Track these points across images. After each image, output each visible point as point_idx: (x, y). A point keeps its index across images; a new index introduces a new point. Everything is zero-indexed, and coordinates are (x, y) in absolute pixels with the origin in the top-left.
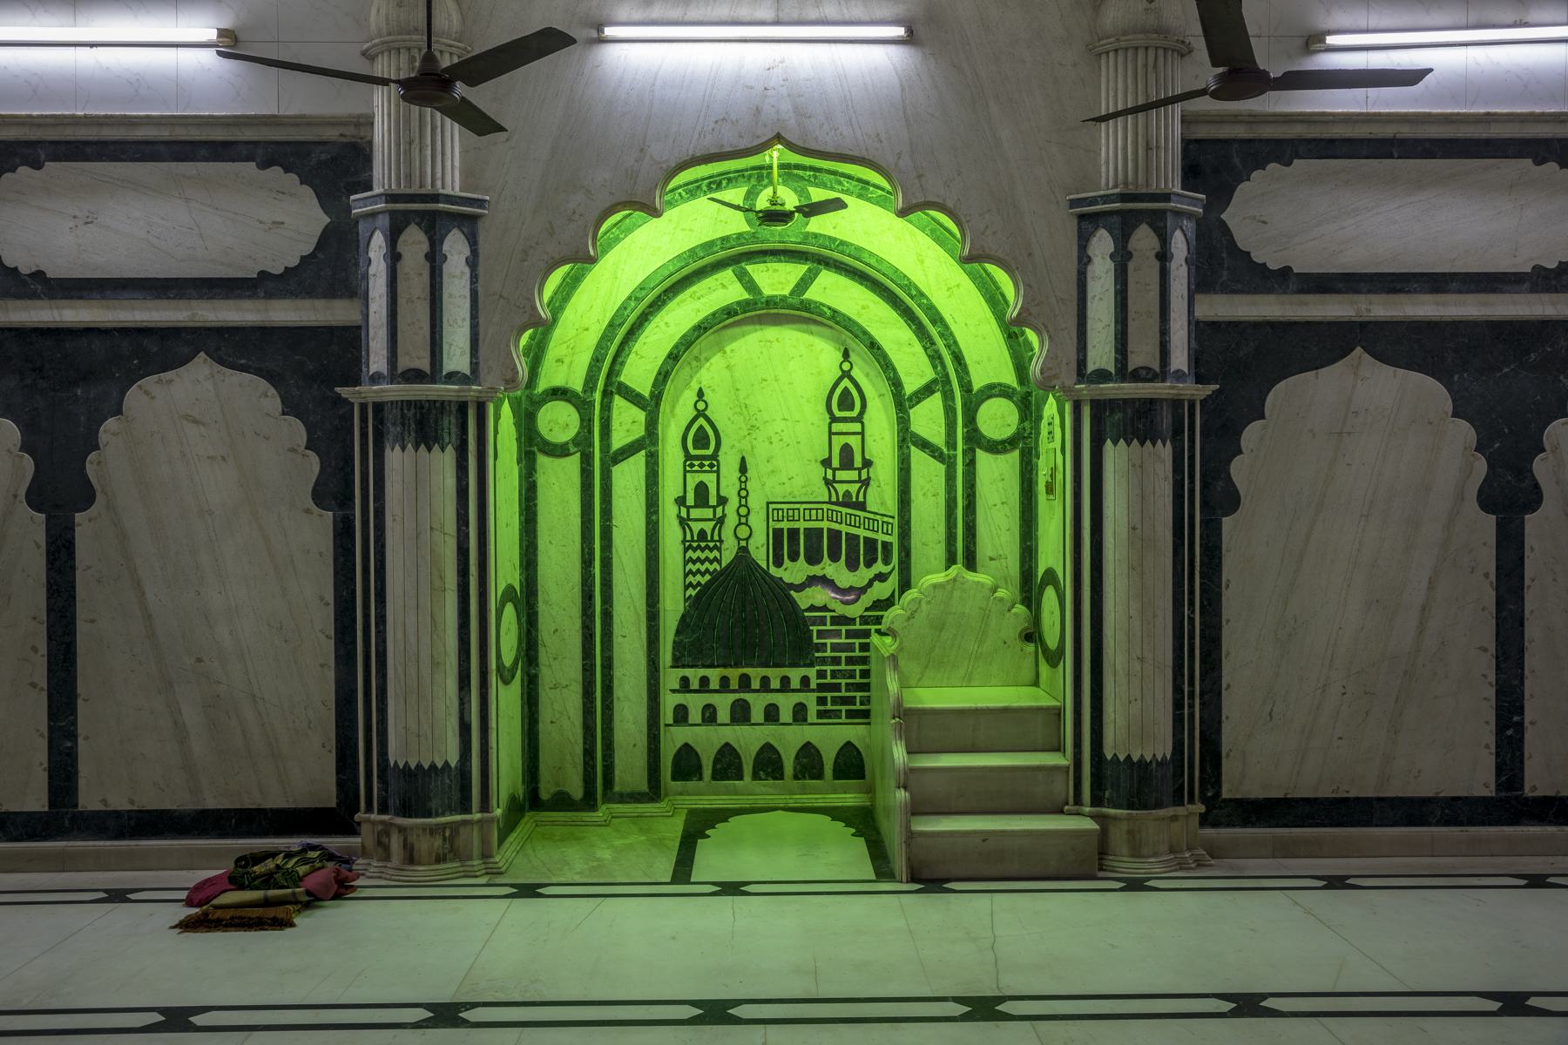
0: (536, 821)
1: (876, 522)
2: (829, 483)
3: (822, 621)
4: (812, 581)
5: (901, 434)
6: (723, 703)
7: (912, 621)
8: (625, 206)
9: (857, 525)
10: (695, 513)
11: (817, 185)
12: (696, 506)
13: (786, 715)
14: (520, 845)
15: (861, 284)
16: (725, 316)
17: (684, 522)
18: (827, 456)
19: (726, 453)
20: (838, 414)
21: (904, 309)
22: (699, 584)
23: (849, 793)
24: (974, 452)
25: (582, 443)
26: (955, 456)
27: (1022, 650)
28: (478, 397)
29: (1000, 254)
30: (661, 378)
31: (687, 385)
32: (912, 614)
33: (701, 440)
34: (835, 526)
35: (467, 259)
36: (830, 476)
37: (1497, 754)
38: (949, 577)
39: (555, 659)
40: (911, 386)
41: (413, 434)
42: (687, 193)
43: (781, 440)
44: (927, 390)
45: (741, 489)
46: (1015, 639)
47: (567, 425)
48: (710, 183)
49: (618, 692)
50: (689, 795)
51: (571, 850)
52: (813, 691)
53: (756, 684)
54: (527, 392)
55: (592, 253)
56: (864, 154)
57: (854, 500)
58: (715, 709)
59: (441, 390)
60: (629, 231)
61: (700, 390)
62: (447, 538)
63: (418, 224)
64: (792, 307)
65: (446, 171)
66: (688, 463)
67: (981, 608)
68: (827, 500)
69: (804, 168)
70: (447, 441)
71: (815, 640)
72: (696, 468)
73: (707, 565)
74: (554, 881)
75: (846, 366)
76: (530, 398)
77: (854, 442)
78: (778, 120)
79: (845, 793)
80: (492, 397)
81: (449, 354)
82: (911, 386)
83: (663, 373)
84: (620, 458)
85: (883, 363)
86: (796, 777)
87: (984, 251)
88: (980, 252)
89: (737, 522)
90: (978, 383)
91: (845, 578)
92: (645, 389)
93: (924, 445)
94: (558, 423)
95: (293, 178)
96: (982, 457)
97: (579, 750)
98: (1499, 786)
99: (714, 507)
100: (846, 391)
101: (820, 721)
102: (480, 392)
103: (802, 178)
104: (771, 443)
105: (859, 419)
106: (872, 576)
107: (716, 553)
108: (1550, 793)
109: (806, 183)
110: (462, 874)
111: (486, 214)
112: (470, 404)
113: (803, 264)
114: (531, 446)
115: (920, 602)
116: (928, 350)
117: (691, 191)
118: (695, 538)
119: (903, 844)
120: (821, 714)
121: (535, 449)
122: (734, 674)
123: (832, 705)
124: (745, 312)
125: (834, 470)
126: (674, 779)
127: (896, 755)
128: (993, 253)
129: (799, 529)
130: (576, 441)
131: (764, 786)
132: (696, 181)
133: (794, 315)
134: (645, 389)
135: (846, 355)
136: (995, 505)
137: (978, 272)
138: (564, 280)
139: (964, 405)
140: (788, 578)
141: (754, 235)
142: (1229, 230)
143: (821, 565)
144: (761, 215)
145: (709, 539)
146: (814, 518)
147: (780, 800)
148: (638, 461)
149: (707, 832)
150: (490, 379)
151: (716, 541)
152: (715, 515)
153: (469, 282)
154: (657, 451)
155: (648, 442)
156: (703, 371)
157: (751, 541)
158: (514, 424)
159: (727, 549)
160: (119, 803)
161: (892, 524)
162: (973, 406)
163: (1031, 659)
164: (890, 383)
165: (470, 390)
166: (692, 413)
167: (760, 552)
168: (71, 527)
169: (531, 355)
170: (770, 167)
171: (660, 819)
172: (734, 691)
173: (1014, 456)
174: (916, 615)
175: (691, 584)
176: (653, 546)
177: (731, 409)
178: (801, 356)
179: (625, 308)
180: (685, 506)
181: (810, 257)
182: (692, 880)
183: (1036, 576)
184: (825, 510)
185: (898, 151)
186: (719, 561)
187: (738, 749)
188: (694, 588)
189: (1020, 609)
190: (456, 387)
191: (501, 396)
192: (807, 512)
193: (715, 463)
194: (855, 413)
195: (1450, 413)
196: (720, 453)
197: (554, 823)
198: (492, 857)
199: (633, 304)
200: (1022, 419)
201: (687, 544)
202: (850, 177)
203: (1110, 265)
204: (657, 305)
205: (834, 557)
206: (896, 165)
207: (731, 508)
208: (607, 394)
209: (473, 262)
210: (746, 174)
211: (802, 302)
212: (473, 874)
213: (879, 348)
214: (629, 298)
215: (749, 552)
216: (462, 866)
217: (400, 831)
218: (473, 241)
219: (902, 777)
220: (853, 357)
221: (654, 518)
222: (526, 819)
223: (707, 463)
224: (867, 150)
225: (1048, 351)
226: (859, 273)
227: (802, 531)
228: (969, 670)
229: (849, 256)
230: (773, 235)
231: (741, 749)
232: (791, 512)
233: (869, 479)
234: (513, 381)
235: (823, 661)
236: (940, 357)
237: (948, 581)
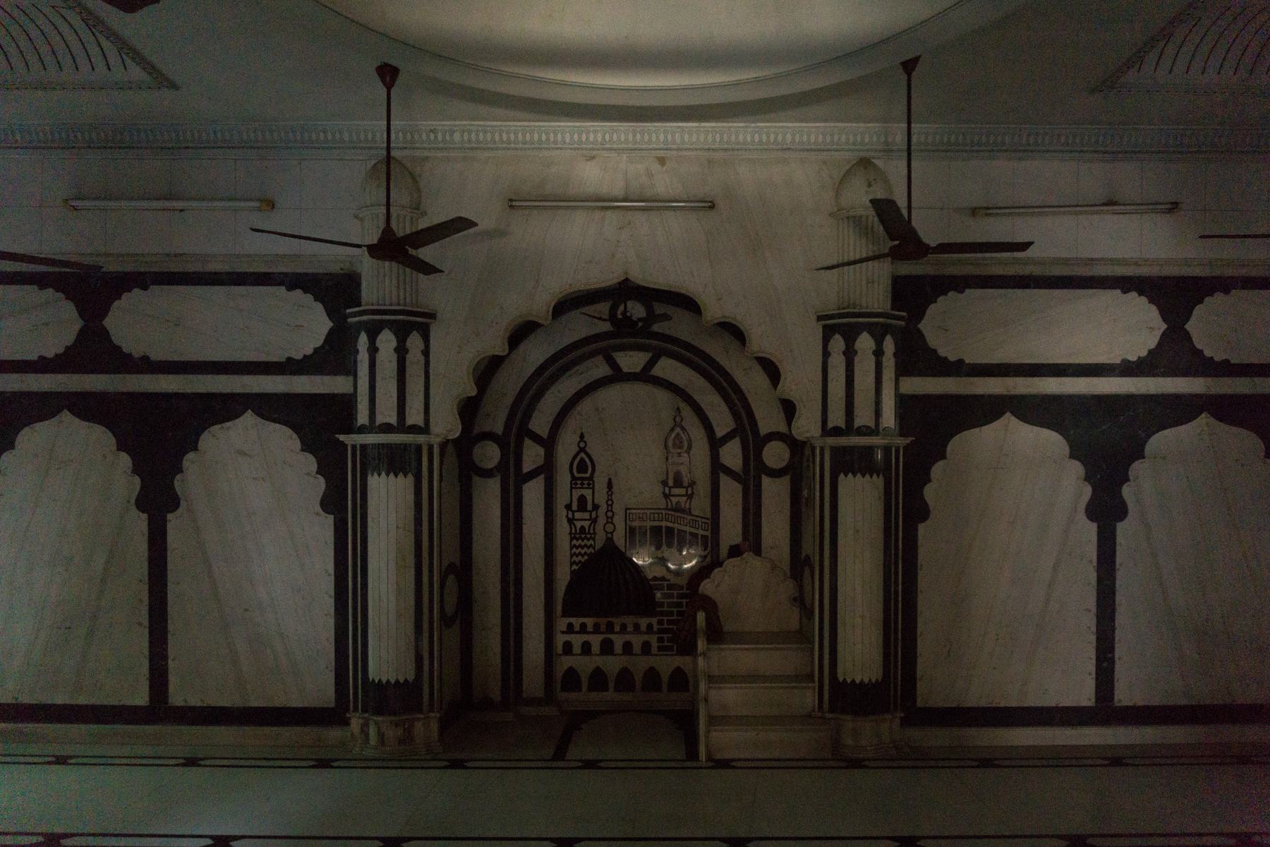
2: (666, 496)
6: (596, 641)
10: (578, 515)
17: (571, 521)
25: (502, 468)
34: (670, 525)
37: (1097, 679)
40: (720, 432)
41: (386, 466)
45: (608, 500)
53: (617, 628)
58: (590, 644)
61: (582, 434)
63: (389, 329)
66: (573, 482)
72: (579, 486)
73: (585, 549)
82: (720, 432)
86: (643, 689)
93: (729, 472)
95: (309, 297)
96: (766, 481)
98: (1097, 699)
100: (582, 460)
101: (659, 653)
108: (1130, 704)
118: (578, 531)
120: (660, 649)
122: (603, 621)
125: (670, 488)
142: (923, 335)
145: (587, 531)
152: (591, 516)
155: (547, 469)
160: (194, 701)
166: (575, 449)
167: (619, 539)
168: (165, 521)
172: (601, 633)
173: (786, 480)
188: (577, 564)
195: (1068, 456)
196: (596, 475)
203: (842, 358)
209: (426, 353)
217: (376, 723)
223: (586, 482)
233: (693, 493)
235: (662, 613)
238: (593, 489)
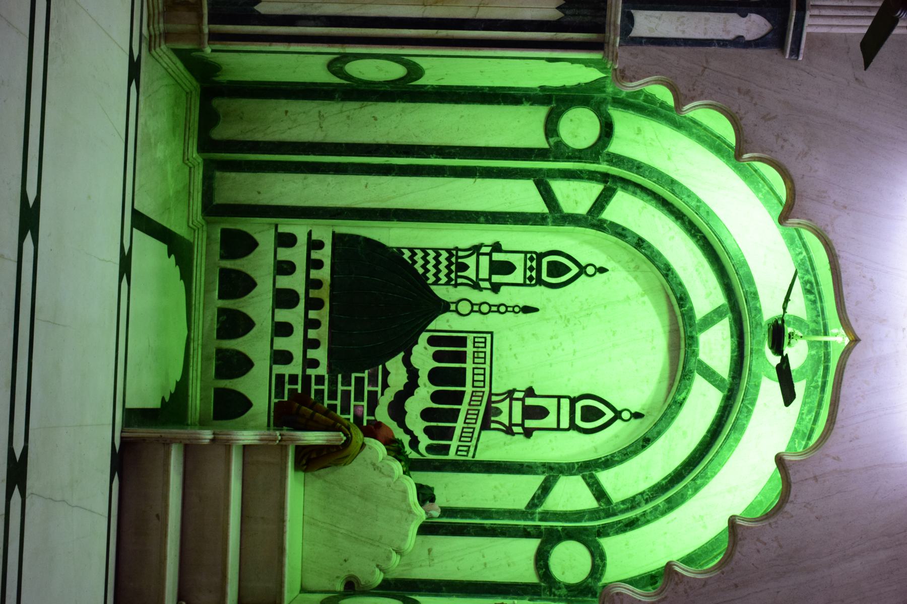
0: (191, 92)
1: (469, 439)
2: (510, 394)
3: (373, 381)
4: (413, 374)
5: (557, 466)
6: (296, 282)
7: (370, 466)
8: (790, 190)
9: (467, 421)
10: (485, 261)
11: (807, 388)
12: (491, 260)
13: (281, 343)
14: (172, 73)
15: (708, 431)
16: (678, 295)
17: (476, 250)
18: (537, 393)
19: (543, 293)
20: (579, 405)
21: (682, 473)
22: (415, 262)
23: (200, 404)
24: (537, 537)
25: (558, 151)
26: (533, 519)
27: (338, 577)
28: (608, 43)
29: (737, 555)
30: (619, 230)
31: (611, 257)
32: (378, 468)
33: (557, 269)
35: (742, 37)
36: (516, 395)
38: (413, 507)
39: (348, 117)
40: (605, 477)
42: (801, 260)
43: (554, 348)
44: (600, 494)
45: (507, 307)
46: (349, 571)
47: (576, 136)
48: (811, 283)
49: (312, 178)
50: (207, 245)
51: (165, 120)
52: (304, 371)
53: (313, 314)
54: (609, 99)
55: (746, 156)
56: (838, 425)
57: (493, 419)
59: (616, 6)
60: (766, 201)
62: (474, 10)
64: (686, 362)
65: (828, 19)
66: (534, 256)
67: (381, 537)
68: (493, 392)
69: (825, 375)
70: (567, 12)
71: (354, 375)
72: (529, 264)
73: (433, 271)
74: (141, 98)
75: (626, 415)
76: (604, 101)
77: (550, 421)
78: (873, 341)
79: (201, 400)
80: (608, 57)
81: (651, 16)
82: (605, 477)
83: (624, 232)
84: (542, 188)
85: (628, 450)
87: (740, 539)
88: (740, 536)
89: (474, 302)
90: (608, 544)
91: (418, 402)
92: (610, 214)
93: (545, 489)
94: (578, 128)
96: (533, 544)
97: (259, 137)
99: (489, 280)
100: (600, 414)
102: (614, 45)
103: (815, 374)
104: (552, 338)
105: (573, 426)
106: (416, 433)
107: (444, 280)
109: (810, 378)
110: (152, 12)
111: (785, 56)
112: (601, 35)
113: (730, 374)
114: (557, 100)
115: (390, 476)
116: (640, 496)
117: (803, 264)
118: (460, 260)
119: (159, 435)
120: (280, 377)
121: (554, 105)
122: (324, 293)
123: (289, 389)
124: (683, 315)
126: (224, 232)
127: (245, 433)
128: (738, 549)
129: (465, 362)
130: (560, 144)
131: (212, 320)
132: (813, 269)
133: (678, 365)
134: (610, 214)
135: (637, 415)
136: (484, 557)
137: (718, 548)
138: (718, 138)
139: (585, 529)
140: (416, 350)
141: (759, 324)
143: (428, 383)
144: (780, 322)
145: (459, 274)
146: (476, 378)
147: (198, 334)
148: (538, 205)
149: (173, 257)
150: (626, 56)
151: (456, 281)
153: (719, 38)
154: (547, 224)
156: (625, 274)
157: (454, 315)
158: (579, 84)
159: (448, 291)
161: (467, 456)
162: (583, 537)
163: (328, 587)
164: (608, 457)
165: (615, 35)
167: (444, 323)
169: (646, 104)
170: (826, 333)
171: (186, 213)
174: (376, 472)
175: (414, 254)
176: (454, 218)
177: (587, 300)
178: (637, 370)
179: (689, 196)
180: (492, 251)
181: (736, 381)
182: (134, 230)
183: (412, 595)
184: (483, 389)
185: (841, 458)
186: (436, 283)
187: (248, 296)
188: (411, 258)
189: (379, 578)
190: (619, 22)
191: (609, 66)
192: (482, 371)
193: (534, 282)
194: (579, 422)
197: (188, 110)
198: (166, 42)
199: (693, 204)
200: (569, 587)
201: (454, 252)
202: (815, 421)
204: (693, 230)
205: (435, 397)
206: (827, 456)
207: (488, 296)
208: (604, 177)
209: (739, 42)
210: (820, 319)
211: (691, 372)
212: (151, 23)
213: (644, 447)
214: (699, 201)
215: (444, 312)
216: (159, 13)
218: (759, 43)
219: (224, 437)
220: (635, 422)
221: (482, 219)
222: (195, 83)
223: (534, 274)
224: (843, 427)
225: (640, 600)
226: (719, 429)
227: (463, 365)
228: (320, 524)
229: (737, 419)
230: (760, 343)
231: (249, 298)
232: (482, 355)
234: (623, 77)
235: (333, 383)
236: (633, 508)
237: (409, 505)
238: (524, 285)
